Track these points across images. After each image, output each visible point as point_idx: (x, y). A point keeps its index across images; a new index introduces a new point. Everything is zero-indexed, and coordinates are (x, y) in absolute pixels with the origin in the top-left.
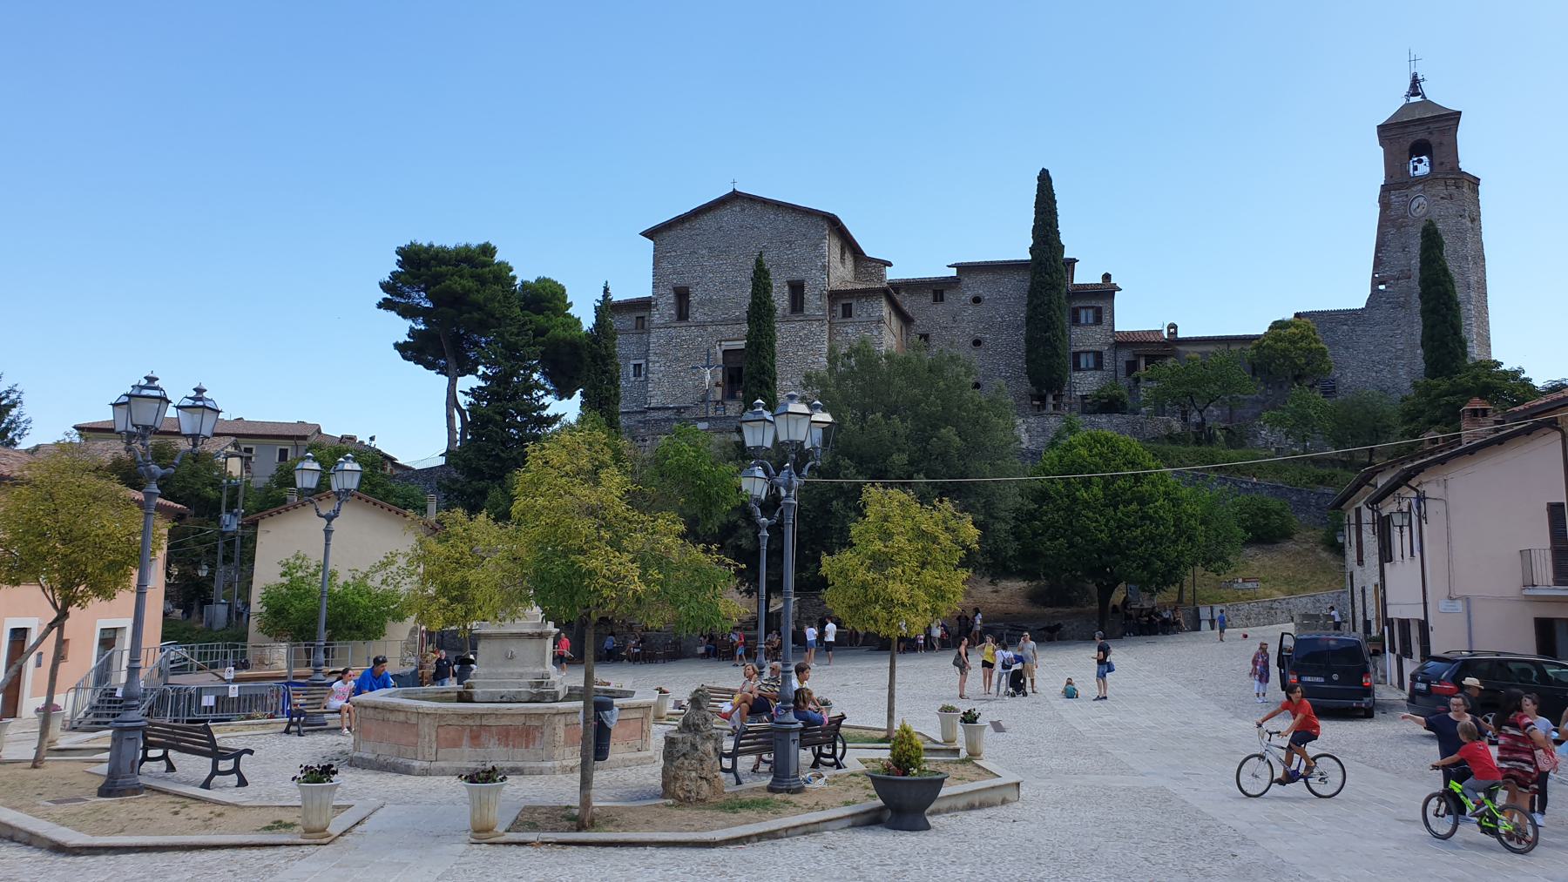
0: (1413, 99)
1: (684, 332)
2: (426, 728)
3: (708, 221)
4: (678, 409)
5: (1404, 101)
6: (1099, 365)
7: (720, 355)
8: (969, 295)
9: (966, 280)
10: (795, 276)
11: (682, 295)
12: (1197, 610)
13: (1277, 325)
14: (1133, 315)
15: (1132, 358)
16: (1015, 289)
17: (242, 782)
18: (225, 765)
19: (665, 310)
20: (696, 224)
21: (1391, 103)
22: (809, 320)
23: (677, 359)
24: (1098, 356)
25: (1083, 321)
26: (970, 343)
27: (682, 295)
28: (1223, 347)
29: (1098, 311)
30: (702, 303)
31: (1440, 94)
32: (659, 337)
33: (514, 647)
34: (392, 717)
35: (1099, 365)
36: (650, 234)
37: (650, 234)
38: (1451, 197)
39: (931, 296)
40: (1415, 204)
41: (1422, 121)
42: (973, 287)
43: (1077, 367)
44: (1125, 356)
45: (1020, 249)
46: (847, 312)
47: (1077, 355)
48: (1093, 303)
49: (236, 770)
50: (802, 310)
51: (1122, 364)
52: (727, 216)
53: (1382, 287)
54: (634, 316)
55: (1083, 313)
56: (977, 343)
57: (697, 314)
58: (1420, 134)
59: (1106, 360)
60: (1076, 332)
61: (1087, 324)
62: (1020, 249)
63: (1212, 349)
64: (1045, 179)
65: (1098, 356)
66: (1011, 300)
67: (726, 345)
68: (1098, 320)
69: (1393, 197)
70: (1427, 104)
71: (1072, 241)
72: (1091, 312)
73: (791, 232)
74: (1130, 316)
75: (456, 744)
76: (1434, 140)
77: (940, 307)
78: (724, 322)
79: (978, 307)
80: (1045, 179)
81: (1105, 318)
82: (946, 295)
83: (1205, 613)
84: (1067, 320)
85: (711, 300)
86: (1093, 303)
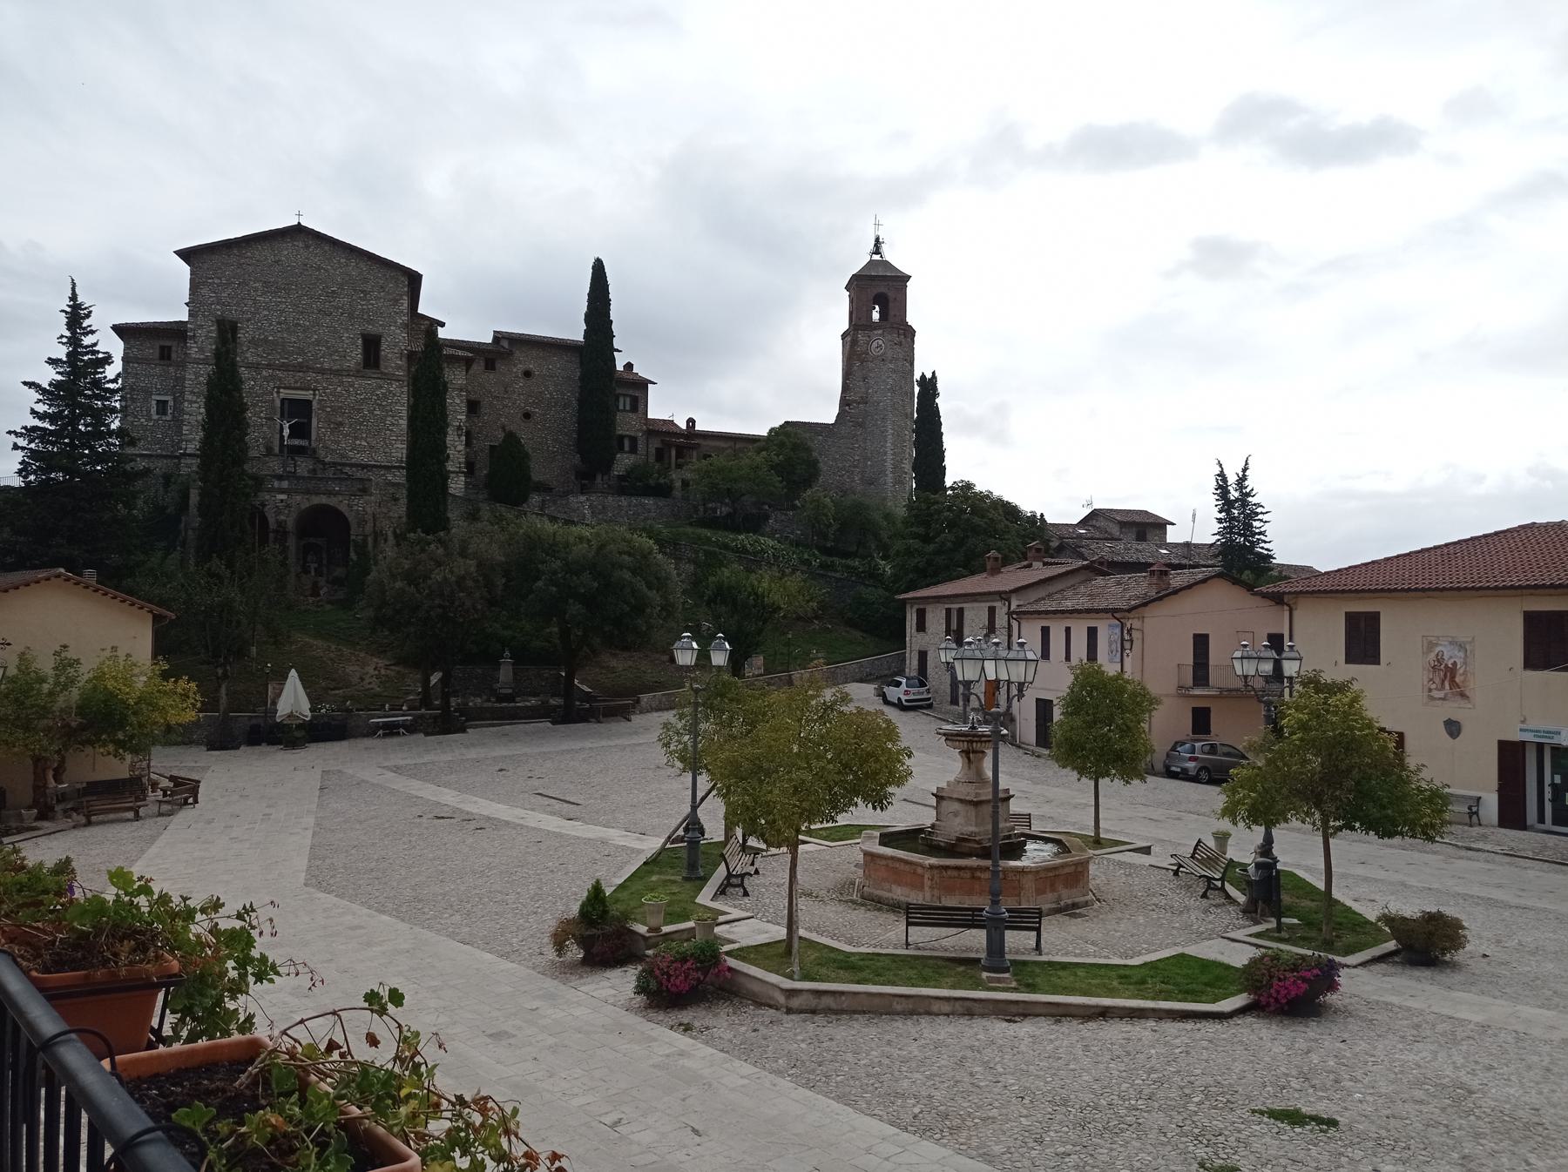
0: (876, 257)
3: (264, 253)
6: (633, 450)
7: (278, 403)
8: (520, 368)
13: (772, 430)
14: (659, 407)
15: (659, 445)
21: (859, 261)
22: (389, 378)
24: (633, 440)
28: (730, 444)
30: (254, 342)
31: (896, 257)
32: (197, 375)
35: (633, 450)
36: (186, 255)
37: (186, 255)
38: (900, 344)
43: (621, 449)
44: (656, 443)
45: (575, 331)
47: (622, 437)
48: (630, 392)
49: (742, 885)
51: (652, 451)
52: (286, 250)
54: (157, 344)
56: (527, 416)
59: (641, 446)
62: (575, 331)
63: (722, 444)
65: (633, 440)
66: (561, 377)
67: (284, 393)
68: (634, 409)
70: (887, 264)
73: (366, 280)
78: (285, 367)
81: (641, 407)
82: (498, 365)
85: (266, 340)
86: (630, 392)
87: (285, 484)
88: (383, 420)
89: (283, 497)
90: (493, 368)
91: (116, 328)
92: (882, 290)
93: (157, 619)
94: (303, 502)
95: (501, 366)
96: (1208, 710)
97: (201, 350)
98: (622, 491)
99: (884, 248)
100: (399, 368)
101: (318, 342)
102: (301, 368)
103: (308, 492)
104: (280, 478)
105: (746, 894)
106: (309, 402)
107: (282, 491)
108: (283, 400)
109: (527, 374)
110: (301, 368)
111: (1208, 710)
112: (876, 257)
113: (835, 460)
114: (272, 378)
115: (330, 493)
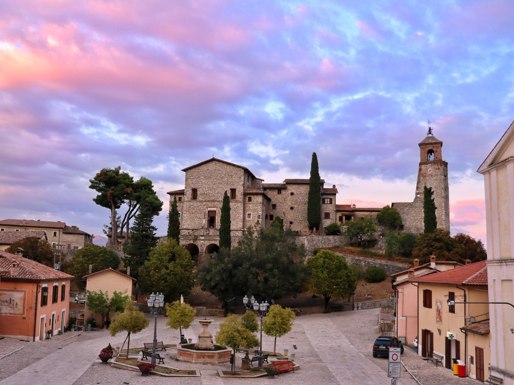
1: (195, 204)
2: (195, 355)
4: (193, 230)
5: (426, 136)
8: (290, 192)
9: (289, 187)
10: (233, 187)
11: (195, 191)
12: (353, 304)
15: (341, 215)
16: (305, 190)
17: (163, 363)
18: (161, 360)
19: (189, 194)
20: (200, 168)
22: (237, 202)
23: (193, 213)
25: (326, 202)
26: (289, 208)
27: (195, 191)
29: (331, 200)
30: (201, 194)
32: (187, 205)
33: (205, 339)
34: (187, 352)
38: (439, 169)
39: (277, 192)
40: (429, 170)
41: (431, 144)
42: (291, 189)
45: (307, 176)
46: (250, 199)
50: (235, 198)
51: (338, 218)
53: (418, 196)
55: (326, 200)
57: (200, 198)
58: (430, 147)
60: (324, 206)
61: (327, 203)
62: (307, 176)
64: (315, 156)
67: (209, 209)
68: (331, 203)
69: (423, 167)
70: (433, 138)
71: (322, 175)
72: (329, 200)
73: (232, 172)
74: (341, 200)
75: (200, 358)
76: (435, 150)
77: (280, 196)
78: (209, 201)
79: (293, 196)
80: (315, 156)
81: (333, 202)
83: (356, 305)
84: (321, 201)
85: (204, 193)
87: (203, 238)
88: (236, 215)
89: (203, 242)
90: (281, 193)
91: (168, 193)
92: (431, 148)
93: (133, 281)
94: (208, 243)
95: (283, 192)
96: (423, 330)
97: (188, 198)
98: (329, 234)
99: (432, 131)
100: (241, 198)
101: (218, 193)
102: (213, 201)
103: (209, 240)
104: (202, 236)
105: (163, 363)
106: (215, 211)
107: (202, 240)
108: (209, 211)
109: (292, 194)
110: (213, 201)
111: (423, 330)
112: (430, 135)
113: (413, 216)
114: (206, 205)
115: (215, 240)
